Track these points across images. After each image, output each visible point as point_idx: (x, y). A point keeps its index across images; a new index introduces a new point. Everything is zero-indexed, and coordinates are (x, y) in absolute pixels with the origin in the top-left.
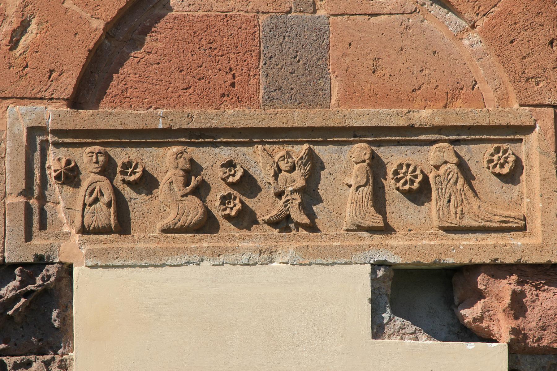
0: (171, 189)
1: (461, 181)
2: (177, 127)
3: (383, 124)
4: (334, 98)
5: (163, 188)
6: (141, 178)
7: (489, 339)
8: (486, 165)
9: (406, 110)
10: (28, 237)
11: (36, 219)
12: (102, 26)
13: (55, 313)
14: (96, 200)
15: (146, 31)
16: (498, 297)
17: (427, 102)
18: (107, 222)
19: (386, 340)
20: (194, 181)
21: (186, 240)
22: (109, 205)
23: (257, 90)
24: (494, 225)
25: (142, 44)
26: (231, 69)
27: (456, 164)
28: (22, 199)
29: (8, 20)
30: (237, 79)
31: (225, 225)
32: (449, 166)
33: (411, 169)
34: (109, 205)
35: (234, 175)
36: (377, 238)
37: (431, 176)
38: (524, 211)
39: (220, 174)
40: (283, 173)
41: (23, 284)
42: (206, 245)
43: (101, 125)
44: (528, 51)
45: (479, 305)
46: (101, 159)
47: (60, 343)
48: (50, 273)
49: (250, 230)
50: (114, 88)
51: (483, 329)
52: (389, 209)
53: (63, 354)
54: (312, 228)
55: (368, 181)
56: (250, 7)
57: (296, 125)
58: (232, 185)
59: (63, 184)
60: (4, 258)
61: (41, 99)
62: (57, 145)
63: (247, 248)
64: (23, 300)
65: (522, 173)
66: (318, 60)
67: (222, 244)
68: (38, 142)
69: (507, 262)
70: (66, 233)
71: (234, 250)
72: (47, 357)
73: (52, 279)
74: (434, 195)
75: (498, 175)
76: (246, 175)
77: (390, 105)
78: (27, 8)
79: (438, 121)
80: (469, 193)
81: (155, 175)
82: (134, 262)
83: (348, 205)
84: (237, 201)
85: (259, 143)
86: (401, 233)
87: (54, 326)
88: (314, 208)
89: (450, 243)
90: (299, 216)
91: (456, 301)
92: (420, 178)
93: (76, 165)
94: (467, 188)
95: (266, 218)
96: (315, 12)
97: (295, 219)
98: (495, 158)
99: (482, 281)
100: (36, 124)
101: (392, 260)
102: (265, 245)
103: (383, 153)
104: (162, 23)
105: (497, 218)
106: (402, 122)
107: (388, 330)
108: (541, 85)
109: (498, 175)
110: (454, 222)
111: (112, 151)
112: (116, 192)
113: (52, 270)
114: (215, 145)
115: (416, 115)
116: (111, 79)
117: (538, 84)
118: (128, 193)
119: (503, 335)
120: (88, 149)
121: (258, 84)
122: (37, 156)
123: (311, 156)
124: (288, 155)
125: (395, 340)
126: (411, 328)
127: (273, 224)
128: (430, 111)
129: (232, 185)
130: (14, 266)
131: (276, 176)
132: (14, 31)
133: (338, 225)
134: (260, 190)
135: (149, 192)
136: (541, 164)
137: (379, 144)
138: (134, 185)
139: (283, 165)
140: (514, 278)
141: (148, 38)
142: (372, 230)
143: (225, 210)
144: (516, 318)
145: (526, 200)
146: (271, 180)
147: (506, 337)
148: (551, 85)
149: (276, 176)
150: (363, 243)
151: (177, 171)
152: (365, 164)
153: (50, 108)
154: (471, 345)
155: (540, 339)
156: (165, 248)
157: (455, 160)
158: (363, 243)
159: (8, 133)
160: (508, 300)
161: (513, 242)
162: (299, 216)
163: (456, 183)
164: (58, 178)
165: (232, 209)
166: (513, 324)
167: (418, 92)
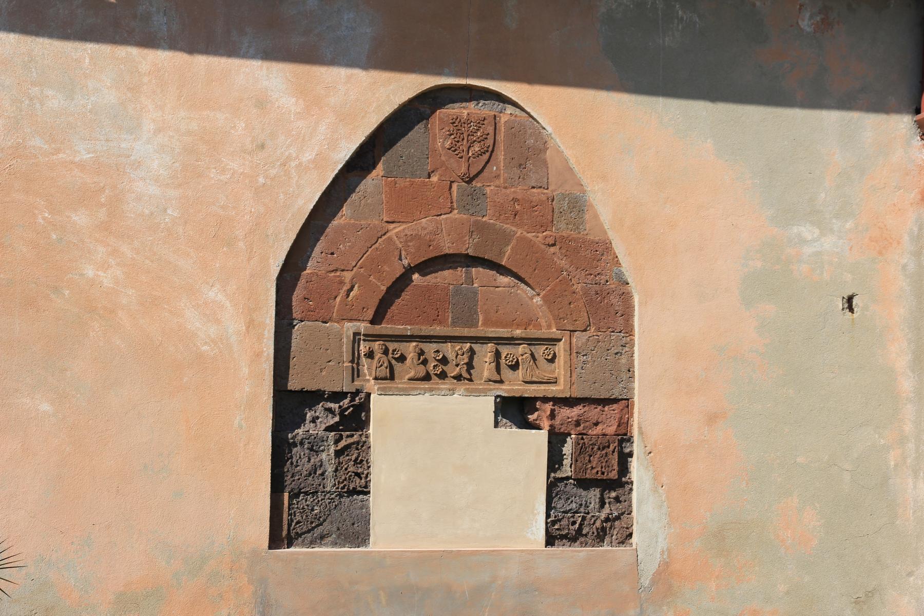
0: (413, 361)
1: (532, 361)
2: (416, 334)
3: (501, 336)
4: (480, 323)
5: (408, 361)
6: (400, 356)
7: (538, 428)
8: (542, 354)
9: (511, 330)
10: (353, 381)
11: (356, 373)
12: (385, 289)
13: (363, 414)
14: (381, 366)
15: (403, 291)
16: (545, 411)
17: (518, 326)
18: (385, 375)
19: (499, 429)
20: (422, 358)
21: (419, 384)
22: (387, 368)
23: (448, 319)
24: (544, 381)
25: (400, 297)
26: (437, 309)
27: (530, 354)
28: (350, 364)
29: (346, 285)
30: (440, 313)
31: (434, 377)
32: (527, 355)
33: (512, 356)
34: (387, 368)
35: (439, 356)
36: (497, 385)
37: (520, 359)
38: (556, 375)
39: (433, 356)
40: (459, 356)
41: (351, 401)
42: (427, 386)
43: (384, 332)
44: (561, 306)
45: (536, 414)
46: (383, 347)
47: (364, 426)
48: (362, 396)
49: (444, 380)
50: (388, 315)
51: (537, 424)
52: (502, 372)
53: (366, 432)
54: (471, 380)
55: (494, 361)
56: (446, 282)
57: (465, 335)
58: (438, 360)
59: (367, 357)
60: (343, 389)
61: (359, 320)
62: (364, 340)
63: (444, 388)
64: (351, 409)
65: (556, 358)
66: (474, 306)
67: (434, 386)
68: (357, 339)
69: (549, 396)
70: (368, 379)
71: (439, 389)
72: (361, 433)
73: (363, 400)
74: (520, 367)
75: (547, 359)
76: (444, 356)
77: (503, 328)
78: (354, 280)
79: (524, 335)
80: (535, 366)
81: (405, 355)
82: (397, 393)
83: (486, 370)
84: (440, 367)
85: (449, 342)
86: (507, 383)
87: (362, 419)
88: (471, 371)
89: (526, 388)
90: (465, 375)
91: (526, 412)
92: (515, 360)
93: (372, 350)
94: (534, 364)
95: (452, 375)
96: (473, 285)
97: (464, 376)
98: (546, 352)
99: (538, 404)
100: (357, 331)
101: (503, 395)
102: (451, 387)
103: (500, 348)
104: (409, 287)
105: (546, 378)
106: (509, 335)
107: (500, 424)
108: (565, 322)
109: (547, 359)
110: (529, 379)
111: (387, 344)
112: (390, 362)
113: (363, 395)
114: (430, 342)
115: (515, 332)
116: (387, 312)
117: (564, 321)
118: (393, 362)
119: (546, 427)
120: (378, 343)
121: (448, 316)
122: (356, 345)
123: (471, 349)
124: (461, 349)
125: (503, 429)
126: (509, 424)
127: (454, 378)
128: (521, 331)
129: (438, 360)
130: (347, 393)
131: (456, 357)
132: (348, 290)
133: (481, 379)
134: (449, 363)
135: (403, 362)
136: (564, 355)
137: (498, 344)
138: (396, 359)
139: (460, 352)
140: (551, 403)
141: (403, 294)
142: (495, 382)
143: (435, 371)
144: (551, 420)
145: (557, 370)
146: (454, 358)
147: (547, 428)
148: (569, 322)
149: (456, 357)
150: (492, 387)
151: (415, 354)
152: (493, 353)
153: (362, 324)
154: (534, 431)
155: (560, 429)
156: (410, 387)
157: (530, 352)
158: (492, 387)
159: (345, 335)
160: (549, 413)
161: (552, 388)
162: (465, 375)
163: (530, 362)
164: (365, 355)
165: (437, 371)
166: (550, 423)
167: (515, 322)
